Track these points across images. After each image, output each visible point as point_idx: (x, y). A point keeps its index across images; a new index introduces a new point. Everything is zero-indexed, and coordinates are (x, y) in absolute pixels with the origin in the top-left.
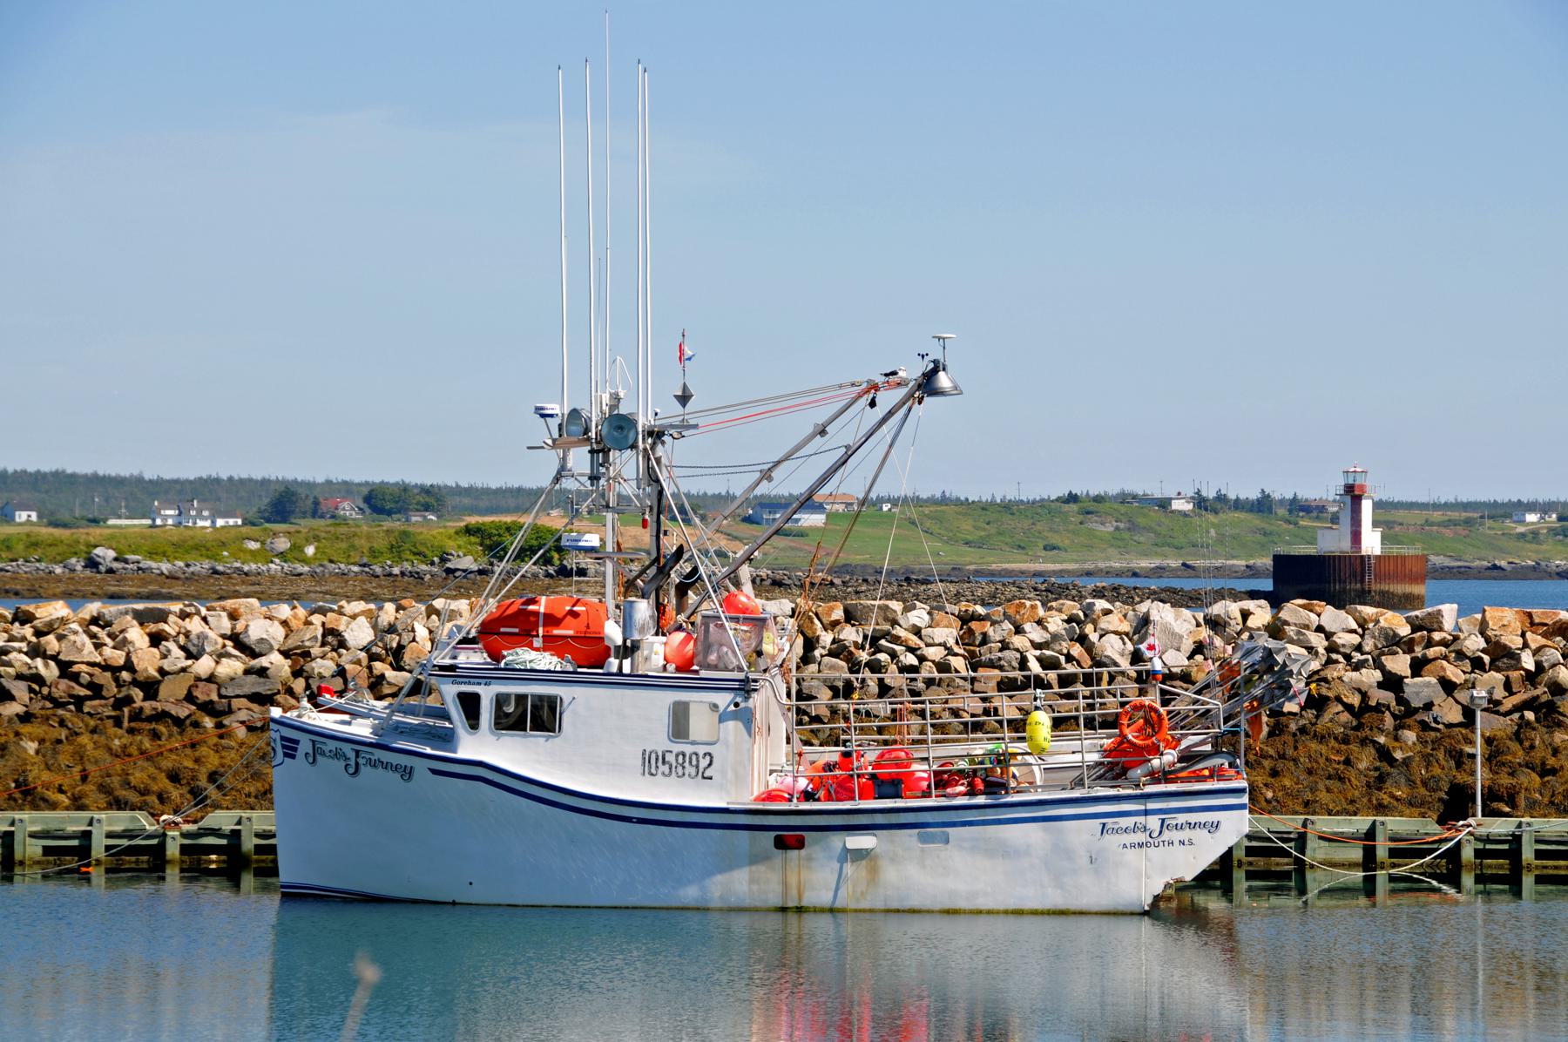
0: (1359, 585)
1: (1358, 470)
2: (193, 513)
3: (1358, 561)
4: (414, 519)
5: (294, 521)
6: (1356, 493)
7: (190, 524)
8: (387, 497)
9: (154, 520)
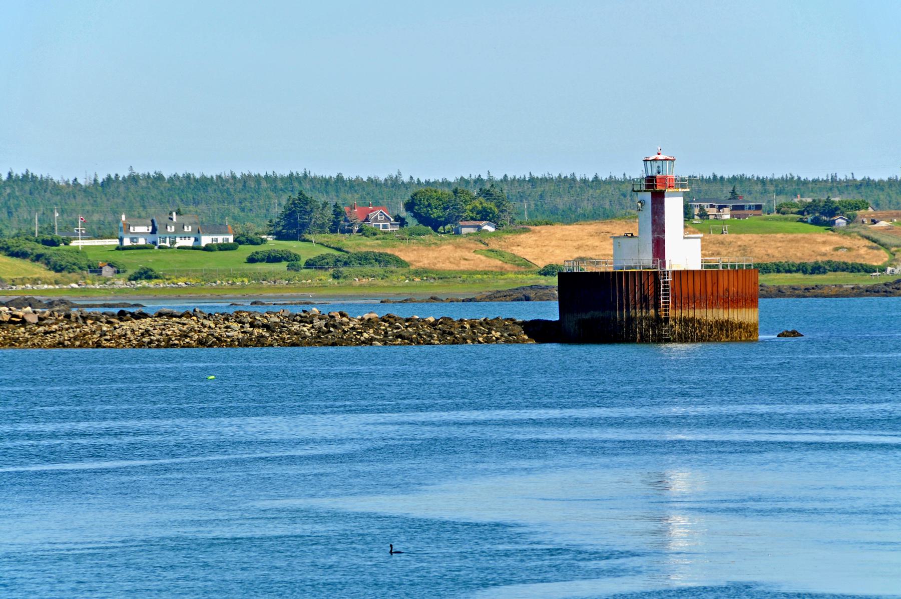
0: (652, 312)
1: (661, 157)
2: (171, 229)
3: (651, 279)
4: (464, 231)
5: (307, 236)
6: (659, 188)
7: (168, 244)
8: (434, 202)
9: (121, 240)
